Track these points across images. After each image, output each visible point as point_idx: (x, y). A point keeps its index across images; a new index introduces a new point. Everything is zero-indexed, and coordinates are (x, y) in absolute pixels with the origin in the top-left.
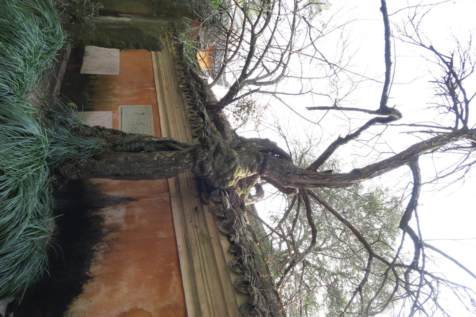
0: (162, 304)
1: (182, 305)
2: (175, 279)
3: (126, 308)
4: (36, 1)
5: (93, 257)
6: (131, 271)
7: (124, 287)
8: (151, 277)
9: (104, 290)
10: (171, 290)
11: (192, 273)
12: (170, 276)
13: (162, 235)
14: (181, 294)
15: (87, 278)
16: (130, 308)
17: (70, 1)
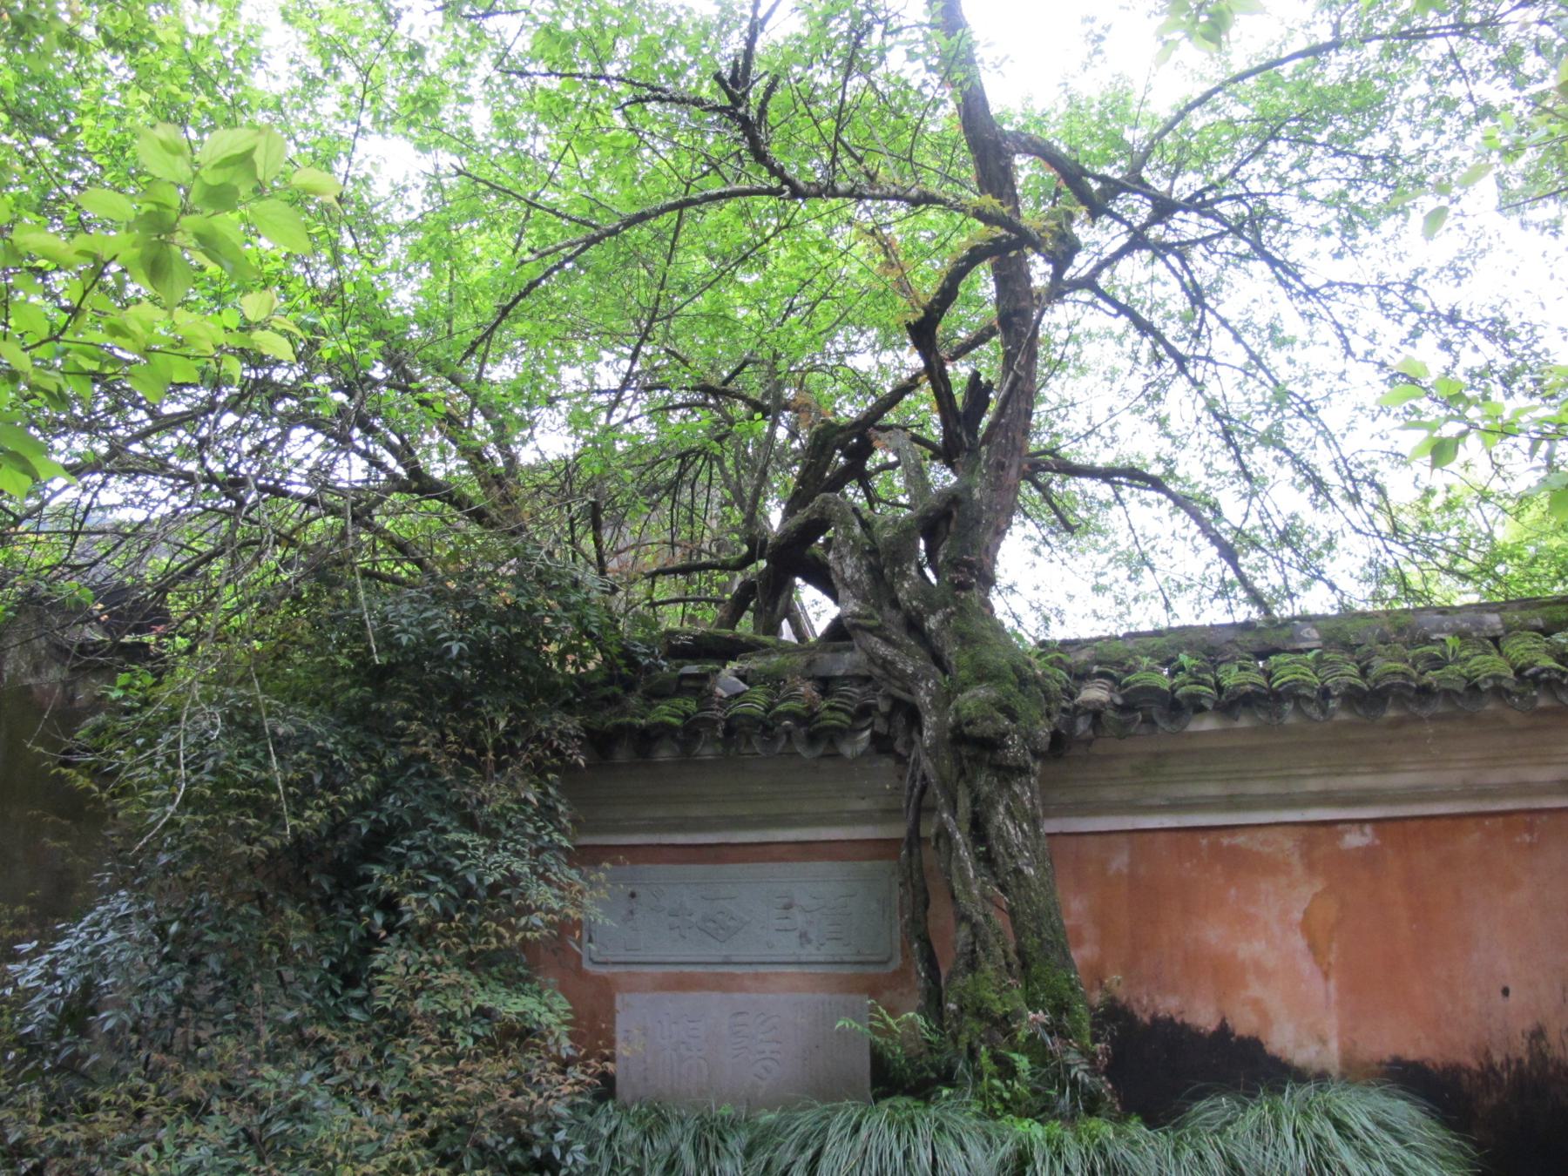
0: (1299, 870)
1: (1305, 830)
2: (1241, 839)
3: (1299, 942)
4: (1410, 1172)
5: (1172, 1019)
6: (1213, 934)
7: (1250, 949)
8: (1233, 891)
9: (1255, 990)
10: (1267, 850)
11: (1232, 803)
12: (1233, 849)
13: (1120, 862)
14: (1279, 829)
15: (1224, 1031)
16: (1299, 935)
17: (126, 1172)
